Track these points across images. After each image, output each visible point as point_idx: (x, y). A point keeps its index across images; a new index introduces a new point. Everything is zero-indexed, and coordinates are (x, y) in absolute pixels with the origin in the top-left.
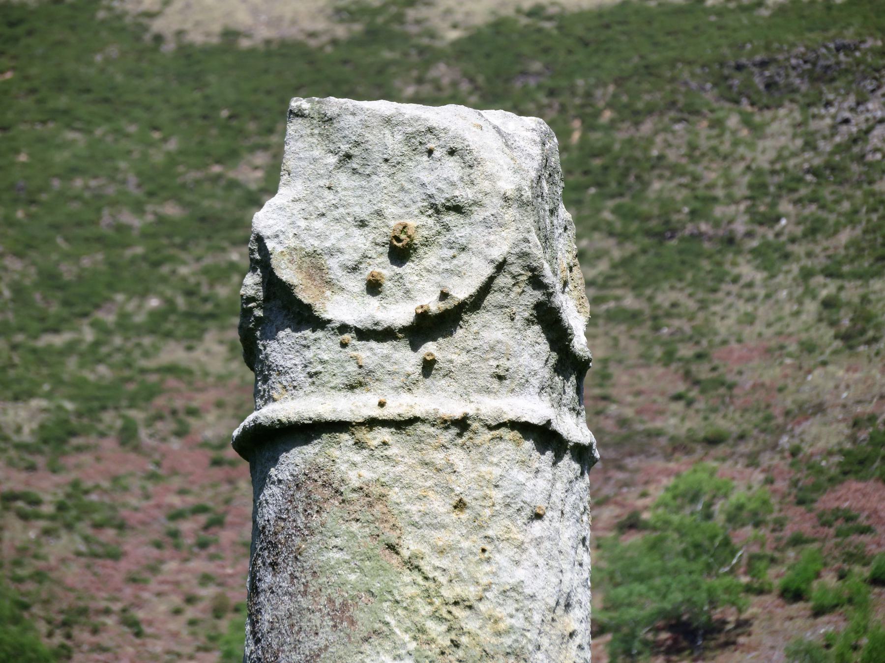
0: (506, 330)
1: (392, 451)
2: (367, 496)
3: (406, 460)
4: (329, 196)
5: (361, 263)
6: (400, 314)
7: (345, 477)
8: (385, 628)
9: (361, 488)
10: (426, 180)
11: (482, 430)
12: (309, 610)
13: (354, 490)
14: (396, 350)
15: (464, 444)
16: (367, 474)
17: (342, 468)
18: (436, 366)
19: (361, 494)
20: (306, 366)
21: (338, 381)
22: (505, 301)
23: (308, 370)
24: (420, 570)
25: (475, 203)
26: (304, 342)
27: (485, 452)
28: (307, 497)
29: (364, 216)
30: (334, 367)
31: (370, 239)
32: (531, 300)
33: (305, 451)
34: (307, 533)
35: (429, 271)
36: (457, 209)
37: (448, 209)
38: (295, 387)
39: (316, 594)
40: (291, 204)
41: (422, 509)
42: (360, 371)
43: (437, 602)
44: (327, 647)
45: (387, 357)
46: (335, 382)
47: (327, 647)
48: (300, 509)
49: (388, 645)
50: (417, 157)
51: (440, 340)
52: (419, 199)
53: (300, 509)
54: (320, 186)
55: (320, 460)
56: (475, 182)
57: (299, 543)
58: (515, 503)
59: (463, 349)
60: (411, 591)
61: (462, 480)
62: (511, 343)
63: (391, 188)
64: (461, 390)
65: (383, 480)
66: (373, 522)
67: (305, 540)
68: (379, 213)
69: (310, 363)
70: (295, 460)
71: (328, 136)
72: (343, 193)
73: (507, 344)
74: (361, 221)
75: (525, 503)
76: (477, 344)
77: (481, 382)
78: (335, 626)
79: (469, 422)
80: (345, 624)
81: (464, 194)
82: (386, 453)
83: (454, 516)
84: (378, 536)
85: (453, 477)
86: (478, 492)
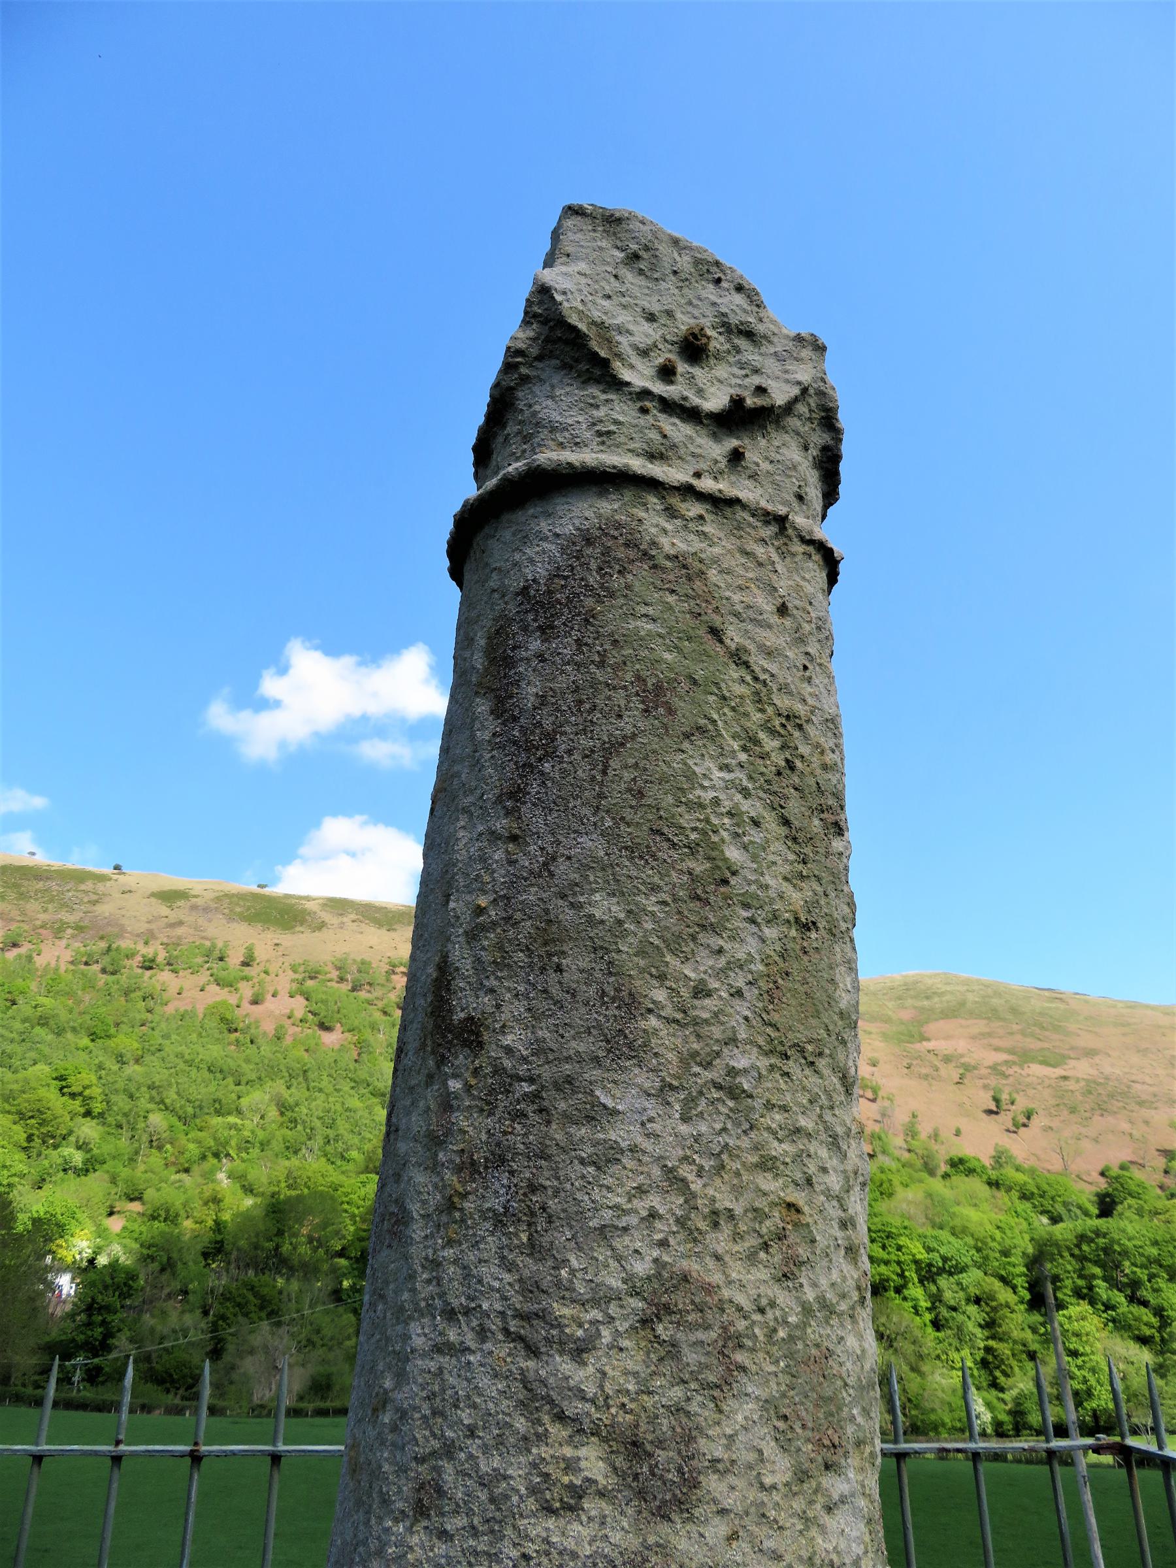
2: (685, 567)
3: (723, 543)
8: (710, 727)
12: (608, 685)
16: (682, 546)
20: (594, 424)
23: (597, 428)
24: (748, 667)
25: (765, 337)
28: (603, 554)
35: (719, 381)
36: (749, 335)
37: (740, 332)
38: (577, 444)
39: (616, 668)
42: (664, 441)
43: (770, 710)
44: (634, 736)
47: (634, 736)
48: (593, 565)
49: (712, 749)
53: (593, 565)
60: (739, 689)
68: (669, 314)
69: (601, 421)
70: (582, 512)
76: (779, 457)
78: (646, 711)
80: (661, 710)
82: (700, 528)
84: (700, 614)
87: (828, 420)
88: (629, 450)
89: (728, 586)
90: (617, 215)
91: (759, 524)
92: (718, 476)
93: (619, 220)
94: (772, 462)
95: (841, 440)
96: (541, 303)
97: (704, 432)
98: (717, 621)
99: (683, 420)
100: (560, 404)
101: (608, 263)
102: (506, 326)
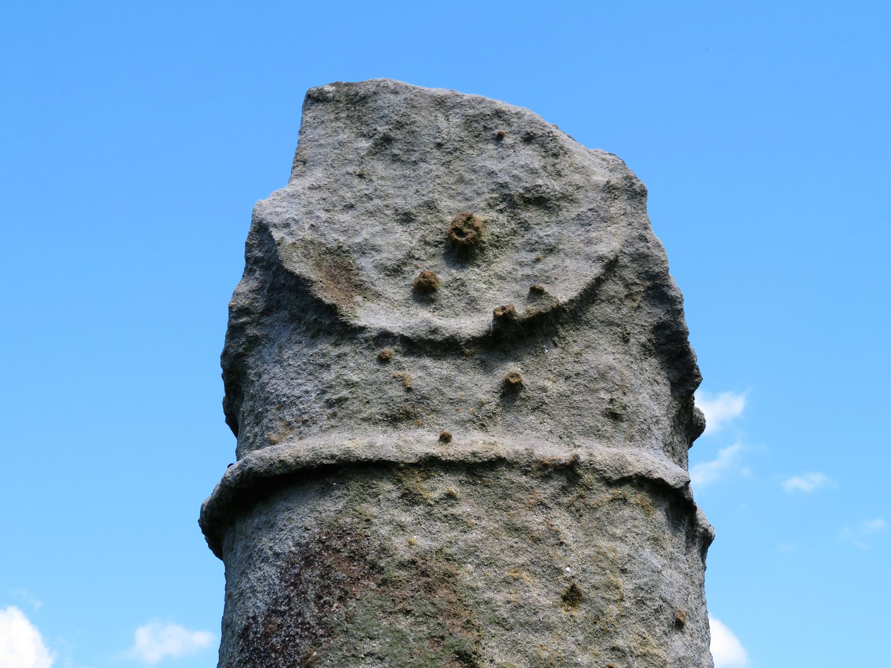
0: (618, 356)
1: (463, 509)
2: (424, 574)
3: (484, 523)
4: (361, 186)
5: (405, 264)
6: (472, 325)
7: (387, 544)
9: (414, 562)
10: (495, 168)
11: (597, 485)
13: (402, 565)
14: (460, 372)
15: (572, 505)
16: (422, 542)
17: (383, 532)
18: (522, 394)
19: (414, 572)
20: (324, 392)
21: (374, 410)
22: (615, 317)
23: (327, 396)
25: (564, 197)
26: (322, 361)
27: (603, 518)
28: (322, 577)
29: (408, 208)
30: (367, 392)
31: (418, 236)
32: (650, 320)
33: (320, 509)
34: (321, 632)
35: (501, 278)
38: (305, 422)
40: (307, 192)
41: (511, 597)
45: (447, 380)
46: (369, 412)
48: (311, 595)
50: (480, 145)
51: (528, 360)
52: (486, 190)
53: (311, 595)
54: (348, 173)
55: (346, 520)
56: (562, 173)
57: (308, 649)
58: (651, 599)
59: (560, 374)
61: (573, 557)
62: (627, 372)
63: (445, 179)
64: (560, 430)
65: (448, 551)
66: (434, 616)
67: (316, 644)
68: (430, 206)
69: (331, 387)
70: (302, 521)
71: (359, 118)
72: (380, 182)
73: (622, 374)
74: (405, 214)
75: (665, 601)
76: (579, 368)
77: (589, 421)
79: (580, 472)
81: (554, 186)
82: (451, 510)
83: (562, 612)
84: (443, 638)
85: (560, 552)
86: (598, 577)
87: (658, 290)
88: (364, 420)
89: (490, 583)
90: (362, 92)
91: (534, 483)
92: (487, 422)
93: (364, 99)
94: (567, 378)
95: (680, 312)
96: (261, 244)
97: (467, 364)
98: (467, 640)
99: (436, 357)
100: (288, 372)
101: (351, 162)
102: (227, 278)
